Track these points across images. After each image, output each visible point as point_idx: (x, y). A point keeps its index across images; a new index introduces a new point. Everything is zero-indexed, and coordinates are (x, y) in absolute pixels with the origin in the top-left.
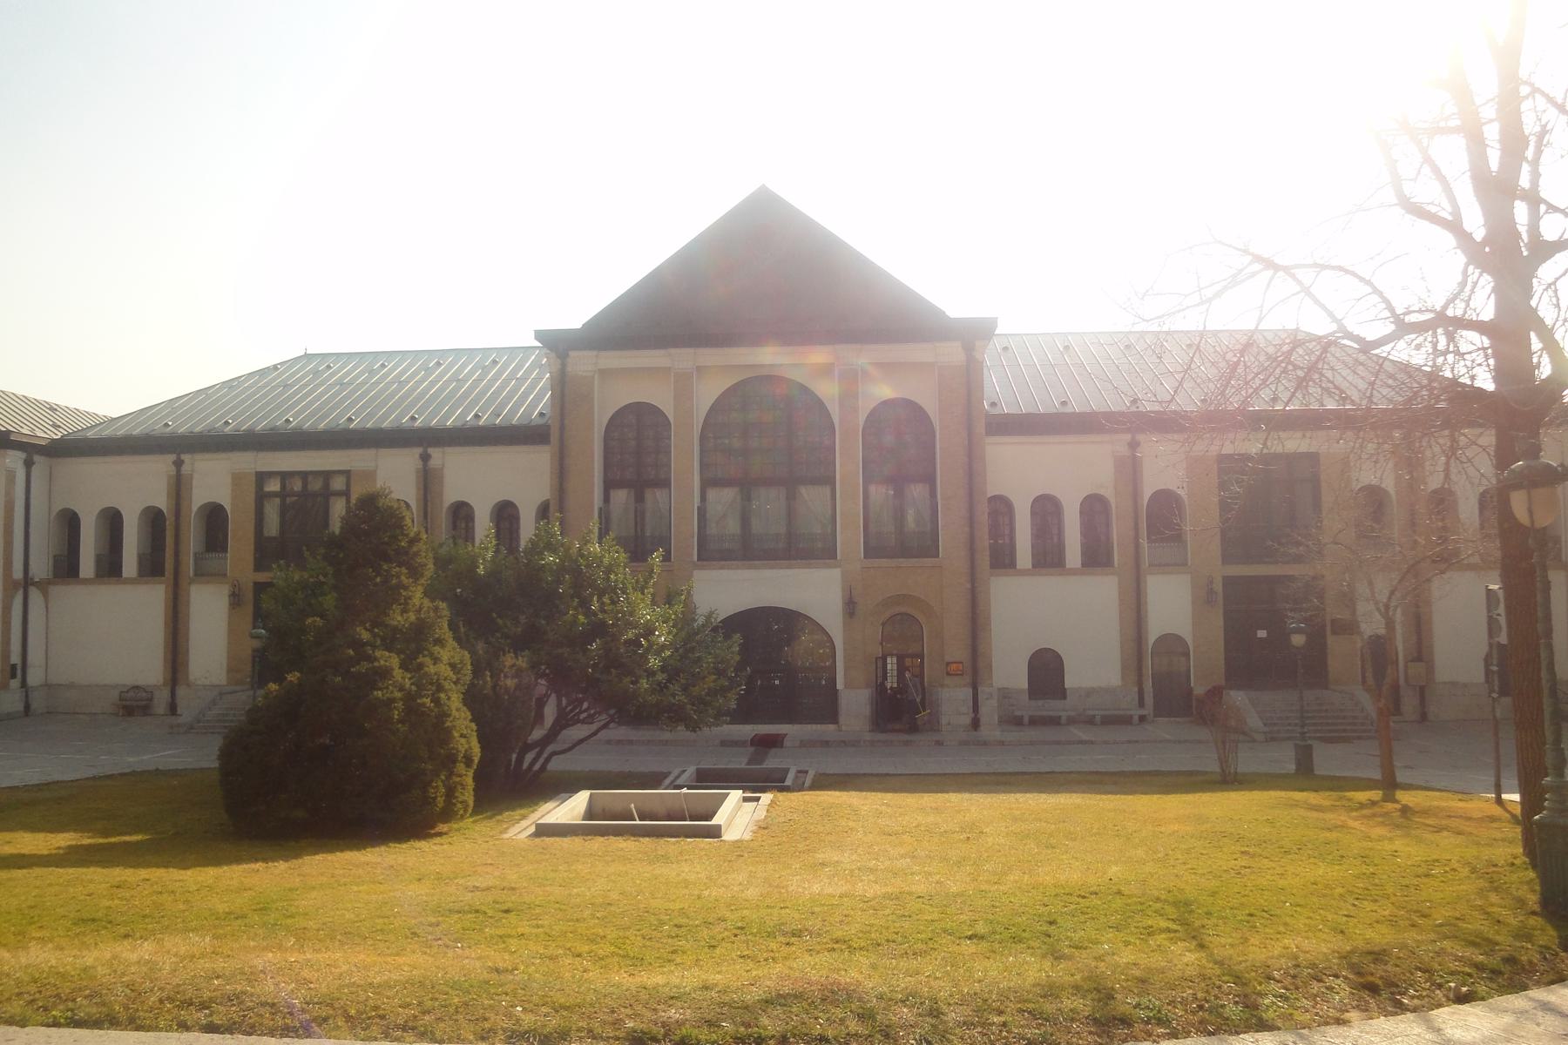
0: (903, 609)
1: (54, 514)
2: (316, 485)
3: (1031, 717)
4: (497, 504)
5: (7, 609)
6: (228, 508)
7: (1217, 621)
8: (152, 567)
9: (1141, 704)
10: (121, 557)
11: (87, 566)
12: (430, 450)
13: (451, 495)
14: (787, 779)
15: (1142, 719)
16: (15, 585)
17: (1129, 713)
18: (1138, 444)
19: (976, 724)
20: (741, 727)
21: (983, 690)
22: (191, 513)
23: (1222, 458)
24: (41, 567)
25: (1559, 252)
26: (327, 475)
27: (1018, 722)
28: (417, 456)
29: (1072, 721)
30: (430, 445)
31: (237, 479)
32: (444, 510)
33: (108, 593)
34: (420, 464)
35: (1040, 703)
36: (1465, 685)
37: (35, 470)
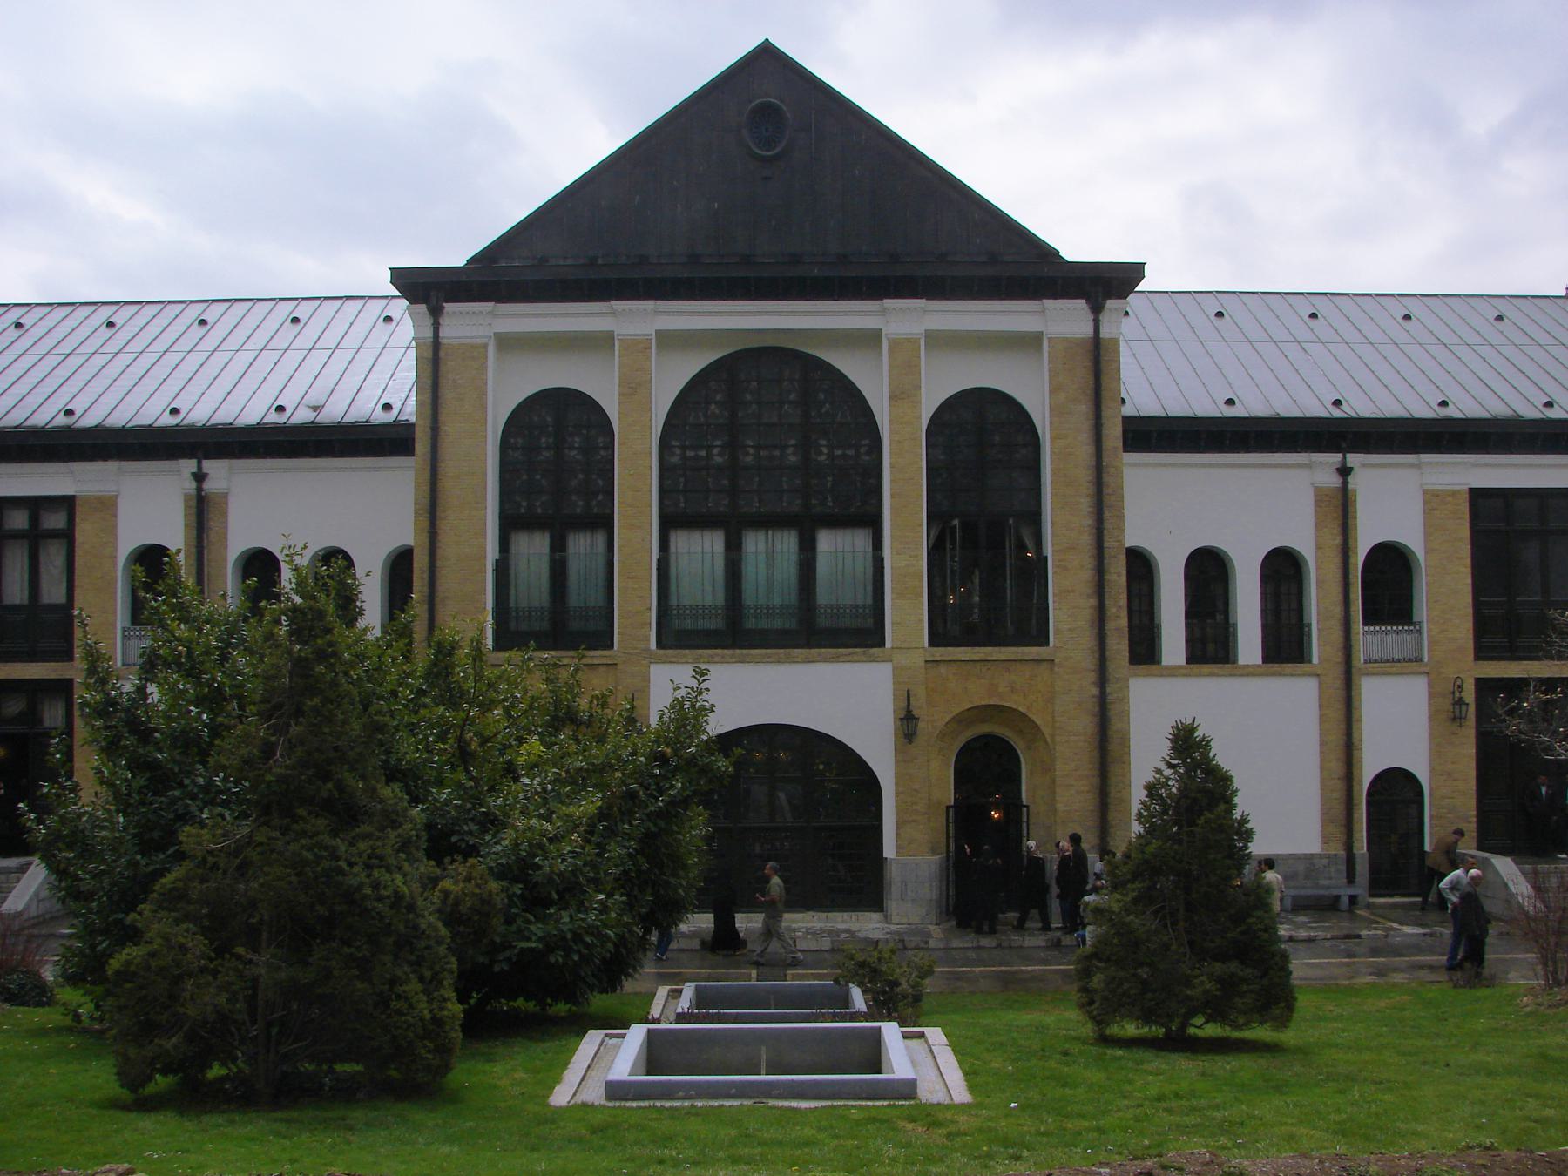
0: (986, 729)
12: (1353, 459)
13: (241, 538)
14: (666, 994)
17: (1335, 892)
23: (1478, 496)
26: (36, 505)
31: (1433, 500)
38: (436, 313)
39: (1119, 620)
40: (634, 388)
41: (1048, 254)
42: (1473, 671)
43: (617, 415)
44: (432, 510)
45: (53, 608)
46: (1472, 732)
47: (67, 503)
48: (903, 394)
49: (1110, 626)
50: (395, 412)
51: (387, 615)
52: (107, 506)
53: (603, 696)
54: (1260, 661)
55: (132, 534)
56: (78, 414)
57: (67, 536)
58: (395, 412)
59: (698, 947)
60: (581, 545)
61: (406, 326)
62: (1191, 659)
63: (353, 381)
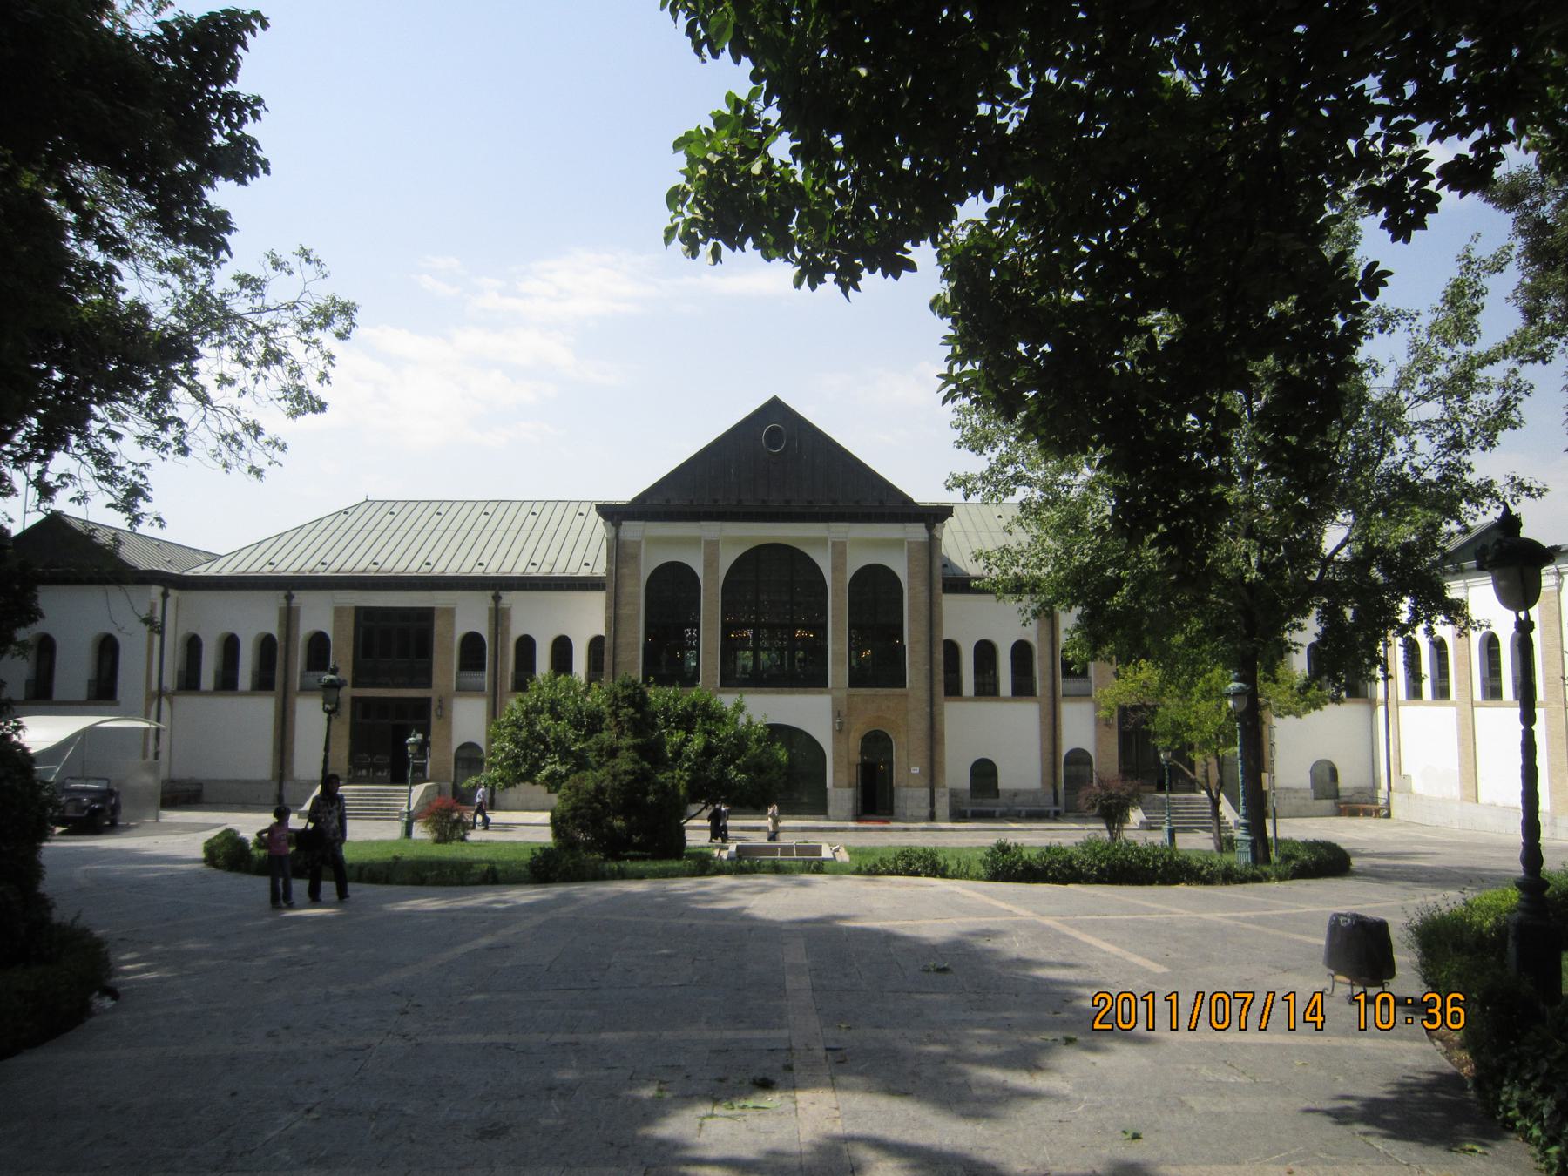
3: (1027, 812)
4: (262, 633)
8: (264, 682)
9: (1056, 802)
11: (208, 678)
13: (516, 630)
15: (1057, 813)
17: (1047, 809)
18: (292, 597)
21: (939, 792)
22: (453, 642)
23: (358, 610)
24: (170, 682)
25: (911, 500)
28: (283, 596)
30: (293, 589)
31: (339, 612)
33: (226, 704)
34: (283, 603)
35: (979, 800)
37: (170, 602)
38: (617, 525)
40: (710, 563)
41: (907, 501)
43: (830, 574)
44: (614, 620)
46: (1116, 731)
49: (936, 679)
51: (1437, 672)
52: (450, 612)
53: (737, 704)
55: (461, 629)
61: (599, 529)
63: (551, 558)
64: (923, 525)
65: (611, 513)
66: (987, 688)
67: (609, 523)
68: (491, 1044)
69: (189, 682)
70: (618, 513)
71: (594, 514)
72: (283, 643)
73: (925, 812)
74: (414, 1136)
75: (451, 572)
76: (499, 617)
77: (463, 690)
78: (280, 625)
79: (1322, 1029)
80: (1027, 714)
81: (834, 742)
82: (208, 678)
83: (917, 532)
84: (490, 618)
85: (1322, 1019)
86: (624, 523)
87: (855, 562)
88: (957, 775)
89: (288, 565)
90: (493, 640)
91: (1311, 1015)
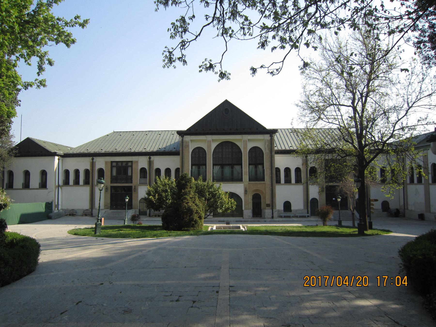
0: (257, 192)
1: (63, 170)
2: (124, 164)
3: (299, 216)
4: (23, 172)
5: (55, 192)
6: (104, 169)
7: (324, 195)
8: (87, 182)
9: (308, 213)
10: (414, 178)
11: (71, 182)
12: (94, 158)
13: (156, 166)
15: (308, 216)
16: (57, 186)
18: (94, 159)
19: (273, 217)
20: (222, 218)
21: (274, 210)
24: (61, 183)
25: (266, 128)
26: (127, 162)
27: (281, 217)
28: (148, 158)
29: (293, 217)
31: (106, 163)
32: (154, 170)
33: (76, 188)
34: (91, 161)
36: (377, 210)
38: (183, 137)
39: (274, 178)
41: (264, 128)
42: (325, 185)
45: (130, 176)
47: (132, 162)
48: (245, 147)
49: (273, 178)
50: (176, 149)
52: (137, 162)
54: (284, 183)
55: (140, 166)
56: (176, 148)
57: (132, 166)
58: (176, 149)
59: (103, 208)
60: (237, 168)
62: (296, 183)
63: (128, 147)
64: (269, 135)
65: (181, 133)
66: (288, 181)
67: (180, 136)
68: (134, 284)
69: (66, 182)
70: (183, 134)
71: (176, 134)
72: (92, 172)
73: (271, 216)
74: (104, 312)
75: (137, 151)
76: (150, 163)
77: (141, 184)
78: (91, 166)
79: (348, 286)
80: (299, 188)
81: (244, 197)
82: (71, 182)
83: (267, 137)
84: (148, 163)
85: (348, 283)
86: (184, 136)
87: (250, 145)
88: (280, 206)
89: (92, 150)
90: (149, 170)
91: (345, 282)
